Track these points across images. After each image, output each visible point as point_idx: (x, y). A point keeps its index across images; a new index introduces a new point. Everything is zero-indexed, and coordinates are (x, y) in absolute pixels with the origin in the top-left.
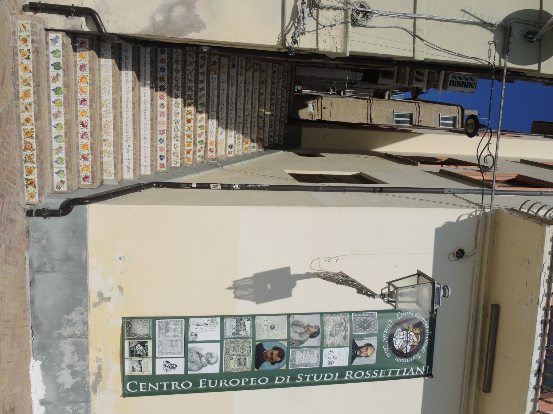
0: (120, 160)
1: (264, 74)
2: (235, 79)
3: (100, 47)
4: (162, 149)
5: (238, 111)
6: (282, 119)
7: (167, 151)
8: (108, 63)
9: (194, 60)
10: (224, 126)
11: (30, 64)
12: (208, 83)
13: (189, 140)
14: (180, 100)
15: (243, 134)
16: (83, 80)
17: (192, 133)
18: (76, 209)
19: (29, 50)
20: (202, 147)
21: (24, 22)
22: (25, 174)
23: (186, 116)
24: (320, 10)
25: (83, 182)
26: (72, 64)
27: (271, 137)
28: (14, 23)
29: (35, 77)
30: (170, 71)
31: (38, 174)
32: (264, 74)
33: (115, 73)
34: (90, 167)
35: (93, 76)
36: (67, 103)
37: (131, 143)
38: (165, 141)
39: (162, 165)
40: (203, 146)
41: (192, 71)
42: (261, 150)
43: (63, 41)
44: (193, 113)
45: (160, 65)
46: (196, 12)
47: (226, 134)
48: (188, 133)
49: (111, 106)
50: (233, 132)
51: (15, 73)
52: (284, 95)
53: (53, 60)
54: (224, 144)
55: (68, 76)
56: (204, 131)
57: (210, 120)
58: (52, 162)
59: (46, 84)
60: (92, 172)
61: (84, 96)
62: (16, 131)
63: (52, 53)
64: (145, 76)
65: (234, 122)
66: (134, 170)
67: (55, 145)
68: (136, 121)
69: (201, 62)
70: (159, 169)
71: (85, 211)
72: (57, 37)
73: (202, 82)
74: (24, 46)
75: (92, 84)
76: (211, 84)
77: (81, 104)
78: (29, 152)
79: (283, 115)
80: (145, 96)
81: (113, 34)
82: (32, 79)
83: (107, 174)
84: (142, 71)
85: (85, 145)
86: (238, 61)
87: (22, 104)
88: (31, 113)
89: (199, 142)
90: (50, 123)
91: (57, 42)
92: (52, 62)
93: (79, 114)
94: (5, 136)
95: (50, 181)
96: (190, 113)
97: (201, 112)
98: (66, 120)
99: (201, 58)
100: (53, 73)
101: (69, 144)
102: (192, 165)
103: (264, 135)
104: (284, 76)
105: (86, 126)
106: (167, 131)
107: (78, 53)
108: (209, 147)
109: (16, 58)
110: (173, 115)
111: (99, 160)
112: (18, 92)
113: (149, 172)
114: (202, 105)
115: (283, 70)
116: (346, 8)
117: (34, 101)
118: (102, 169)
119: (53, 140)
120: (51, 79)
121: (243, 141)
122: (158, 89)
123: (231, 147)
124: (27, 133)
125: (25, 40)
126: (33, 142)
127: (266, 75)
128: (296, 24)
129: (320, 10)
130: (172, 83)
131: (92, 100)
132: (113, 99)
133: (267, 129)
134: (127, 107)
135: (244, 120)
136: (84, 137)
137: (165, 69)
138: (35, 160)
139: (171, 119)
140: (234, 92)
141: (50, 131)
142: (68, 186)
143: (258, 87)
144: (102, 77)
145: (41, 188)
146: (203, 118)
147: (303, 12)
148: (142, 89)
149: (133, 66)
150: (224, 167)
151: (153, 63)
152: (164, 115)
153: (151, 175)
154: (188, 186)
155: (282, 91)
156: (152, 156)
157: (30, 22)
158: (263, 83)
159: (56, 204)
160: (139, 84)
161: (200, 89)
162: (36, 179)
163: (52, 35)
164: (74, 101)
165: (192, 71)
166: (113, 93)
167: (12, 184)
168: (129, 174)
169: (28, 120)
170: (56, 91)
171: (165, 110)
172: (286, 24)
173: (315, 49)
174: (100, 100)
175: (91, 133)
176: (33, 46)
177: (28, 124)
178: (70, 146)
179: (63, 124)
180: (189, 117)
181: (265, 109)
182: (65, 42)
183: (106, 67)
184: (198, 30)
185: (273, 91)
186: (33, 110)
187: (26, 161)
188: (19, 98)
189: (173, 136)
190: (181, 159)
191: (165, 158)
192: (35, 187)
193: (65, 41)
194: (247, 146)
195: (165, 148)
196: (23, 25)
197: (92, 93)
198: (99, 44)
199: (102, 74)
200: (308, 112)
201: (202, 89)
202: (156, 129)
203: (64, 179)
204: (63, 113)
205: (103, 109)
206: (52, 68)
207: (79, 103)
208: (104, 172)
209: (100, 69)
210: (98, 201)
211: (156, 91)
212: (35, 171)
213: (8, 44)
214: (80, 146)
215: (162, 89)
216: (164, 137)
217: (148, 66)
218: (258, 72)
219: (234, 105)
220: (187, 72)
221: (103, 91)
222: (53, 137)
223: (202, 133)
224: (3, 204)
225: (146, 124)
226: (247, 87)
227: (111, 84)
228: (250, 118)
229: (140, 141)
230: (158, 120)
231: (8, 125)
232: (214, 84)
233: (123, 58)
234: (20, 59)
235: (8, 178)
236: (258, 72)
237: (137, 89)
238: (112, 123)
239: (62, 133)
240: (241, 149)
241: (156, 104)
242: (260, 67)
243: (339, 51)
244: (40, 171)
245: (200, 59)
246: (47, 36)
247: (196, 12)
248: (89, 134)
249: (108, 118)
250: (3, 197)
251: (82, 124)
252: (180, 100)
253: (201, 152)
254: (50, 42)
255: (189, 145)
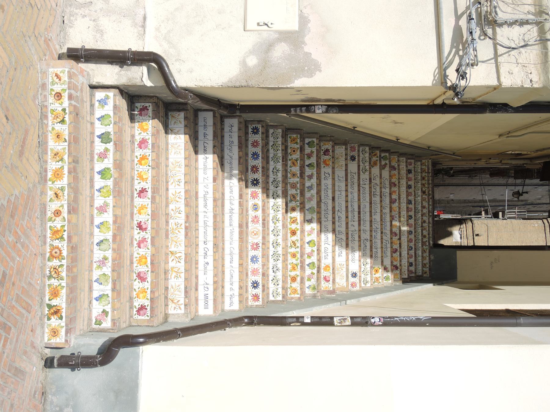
0: (194, 284)
1: (396, 172)
2: (356, 177)
3: (168, 118)
4: (255, 272)
5: (362, 222)
6: (425, 240)
7: (263, 275)
8: (179, 141)
9: (298, 146)
10: (344, 244)
11: (64, 130)
12: (319, 178)
13: (294, 261)
14: (280, 202)
15: (371, 256)
16: (143, 162)
17: (299, 250)
18: (123, 353)
19: (64, 110)
20: (313, 273)
21: (58, 70)
22: (47, 298)
23: (289, 226)
24: (497, 29)
25: (136, 317)
26: (127, 138)
27: (411, 264)
28: (44, 73)
29: (72, 148)
30: (266, 159)
31: (68, 296)
32: (396, 172)
33: (189, 155)
34: (149, 291)
35: (158, 156)
36: (118, 193)
37: (210, 259)
38: (260, 260)
39: (256, 297)
40: (315, 271)
41: (296, 160)
42: (399, 283)
43: (115, 101)
44: (299, 221)
45: (251, 150)
46: (306, 49)
47: (347, 255)
48: (293, 250)
49: (183, 201)
50: (357, 254)
51: (42, 144)
52: (425, 204)
53: (99, 129)
54: (345, 270)
55: (121, 152)
56: (315, 249)
57: (323, 235)
58: (90, 281)
59: (88, 163)
60: (152, 300)
61: (143, 185)
62: (38, 229)
63: (99, 119)
64: (231, 163)
65: (357, 238)
66: (215, 300)
67: (98, 255)
68: (218, 227)
69: (308, 150)
70: (251, 303)
71: (137, 357)
72: (107, 97)
73: (310, 177)
74: (57, 105)
75: (156, 166)
76: (323, 181)
77: (140, 196)
78: (55, 263)
79: (425, 233)
80: (231, 192)
81: (186, 89)
82: (67, 151)
83: (174, 305)
84: (226, 157)
85: (142, 258)
86: (359, 151)
87: (51, 189)
88: (63, 202)
89: (308, 265)
90: (92, 222)
91: (106, 104)
92: (98, 132)
93: (135, 211)
94: (20, 233)
95: (86, 312)
96: (294, 221)
97: (310, 221)
98: (115, 216)
99: (308, 144)
100: (99, 148)
101: (118, 251)
102: (299, 298)
103: (400, 261)
104: (423, 178)
105: (146, 229)
106: (263, 244)
107: (137, 125)
108: (323, 273)
109: (45, 121)
110: (271, 222)
111: (162, 282)
112: (46, 171)
113: (236, 306)
114: (311, 210)
115: (421, 169)
116: (540, 19)
117: (69, 184)
118: (166, 298)
119: (95, 246)
120: (96, 157)
121: (371, 267)
122: (250, 183)
123: (354, 275)
124: (55, 232)
125: (59, 96)
126: (64, 246)
127: (399, 173)
128: (461, 53)
129: (497, 29)
130: (268, 176)
131: (155, 190)
132: (186, 191)
133: (405, 253)
134: (205, 206)
135: (371, 236)
136: (142, 245)
137: (258, 156)
138: (64, 274)
139: (268, 229)
140: (356, 195)
141: (92, 234)
142: (113, 320)
143: (388, 190)
144: (171, 160)
145: (71, 320)
146: (313, 229)
147: (471, 33)
148: (227, 182)
149: (214, 147)
150: (348, 302)
151: (243, 145)
152: (258, 221)
153: (240, 310)
154: (298, 322)
155: (423, 199)
156: (241, 280)
157: (67, 70)
158: (395, 185)
159: (91, 346)
160: (223, 175)
161: (308, 187)
162: (64, 305)
163: (100, 95)
164: (129, 193)
165: (296, 160)
166: (186, 182)
167: (24, 311)
168: (206, 307)
169: (57, 213)
170: (103, 173)
171: (259, 213)
172: (446, 54)
173: (495, 88)
174: (167, 194)
175: (153, 238)
176: (70, 104)
177: (57, 219)
178: (120, 257)
179: (111, 222)
180: (294, 226)
181: (400, 221)
182: (117, 104)
183: (176, 146)
184: (310, 74)
185: (410, 198)
186: (66, 197)
187: (50, 277)
188: (46, 181)
189: (271, 253)
190: (283, 288)
191: (260, 286)
192: (61, 318)
193: (117, 101)
194: (377, 275)
195: (261, 271)
196: (57, 75)
197: (156, 180)
198: (167, 115)
199: (170, 156)
200: (456, 237)
201: (310, 188)
202: (247, 241)
203: (108, 308)
204: (111, 206)
205: (171, 206)
206: (97, 141)
207: (136, 195)
208: (170, 303)
209: (167, 149)
210: (158, 341)
211: (247, 187)
212: (63, 292)
213: (34, 101)
214: (135, 260)
215: (255, 183)
216: (259, 253)
217: (236, 149)
218: (387, 168)
219: (356, 214)
220: (289, 162)
221: (172, 181)
222: (95, 243)
223: (313, 251)
224: (6, 340)
225: (232, 233)
226: (373, 190)
227: (183, 170)
228: (379, 234)
229: (223, 259)
230: (250, 228)
231: (26, 218)
232: (327, 183)
233: (201, 136)
234: (50, 124)
235: (18, 299)
236: (387, 168)
237: (219, 181)
238: (183, 226)
239: (109, 235)
240: (369, 279)
241: (247, 205)
242: (390, 162)
243: (536, 86)
244: (71, 292)
245: (306, 146)
246: (92, 96)
247: (306, 49)
248: (149, 241)
249: (178, 219)
250: (7, 329)
251: (140, 226)
252: (280, 202)
253: (312, 280)
254: (97, 104)
255: (294, 269)
